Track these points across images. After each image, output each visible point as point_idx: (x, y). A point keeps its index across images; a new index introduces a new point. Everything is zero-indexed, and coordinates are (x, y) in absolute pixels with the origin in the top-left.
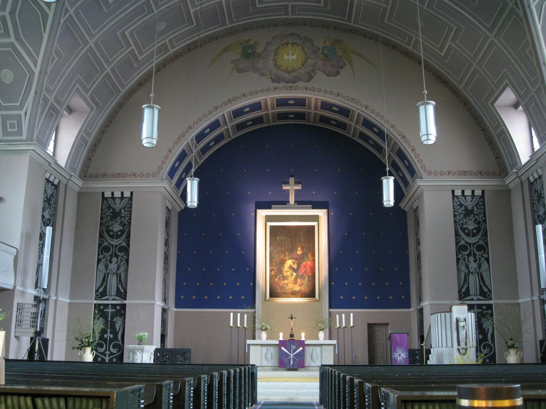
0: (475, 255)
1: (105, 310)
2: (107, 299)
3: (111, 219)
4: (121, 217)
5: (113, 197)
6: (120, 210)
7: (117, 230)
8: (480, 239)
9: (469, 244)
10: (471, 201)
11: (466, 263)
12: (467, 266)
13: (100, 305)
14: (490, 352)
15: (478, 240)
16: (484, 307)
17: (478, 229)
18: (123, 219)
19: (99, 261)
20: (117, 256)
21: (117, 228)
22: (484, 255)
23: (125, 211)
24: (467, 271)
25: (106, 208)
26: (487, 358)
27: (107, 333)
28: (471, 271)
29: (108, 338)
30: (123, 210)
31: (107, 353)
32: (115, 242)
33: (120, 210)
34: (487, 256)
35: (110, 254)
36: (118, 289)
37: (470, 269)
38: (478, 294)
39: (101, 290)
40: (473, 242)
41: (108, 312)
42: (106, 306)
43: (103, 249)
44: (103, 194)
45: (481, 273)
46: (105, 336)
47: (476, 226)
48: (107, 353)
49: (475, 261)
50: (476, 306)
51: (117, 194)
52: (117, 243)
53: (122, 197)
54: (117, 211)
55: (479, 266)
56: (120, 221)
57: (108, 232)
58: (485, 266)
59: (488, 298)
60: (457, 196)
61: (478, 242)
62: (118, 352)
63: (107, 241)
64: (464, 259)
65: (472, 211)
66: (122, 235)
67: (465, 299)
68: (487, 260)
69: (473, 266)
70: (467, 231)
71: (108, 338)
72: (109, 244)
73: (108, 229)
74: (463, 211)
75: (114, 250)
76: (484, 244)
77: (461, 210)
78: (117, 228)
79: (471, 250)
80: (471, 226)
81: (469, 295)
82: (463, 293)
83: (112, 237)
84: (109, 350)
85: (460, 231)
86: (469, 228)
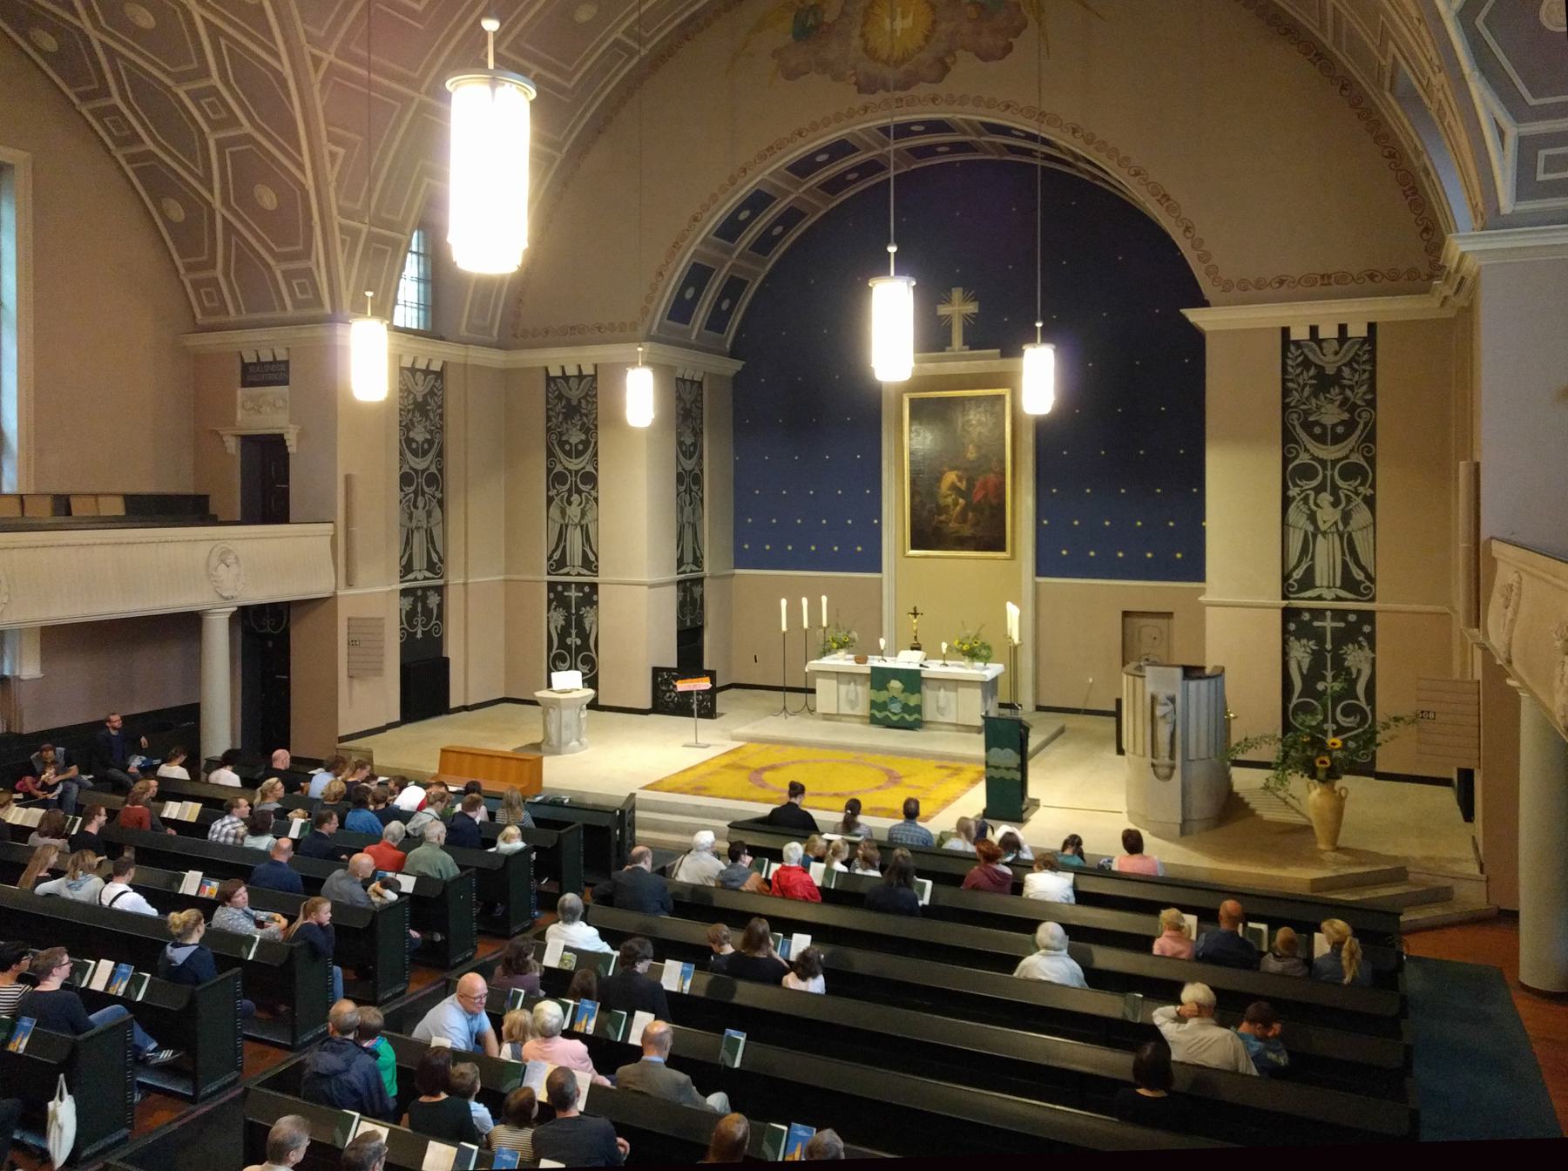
0: (1335, 490)
1: (1316, 624)
2: (568, 574)
4: (1343, 387)
5: (565, 378)
8: (1352, 451)
9: (1323, 462)
12: (1312, 518)
17: (1350, 426)
18: (1348, 392)
19: (550, 500)
20: (579, 492)
21: (575, 437)
22: (1361, 489)
23: (1354, 370)
27: (1324, 678)
28: (1323, 527)
30: (1346, 372)
32: (1329, 453)
33: (1339, 370)
36: (584, 552)
37: (1320, 523)
38: (1338, 583)
39: (556, 556)
42: (567, 585)
44: (1285, 332)
45: (1350, 535)
46: (1320, 686)
49: (1335, 504)
50: (1328, 614)
51: (1328, 332)
53: (581, 377)
54: (1330, 370)
55: (1346, 517)
57: (1308, 426)
58: (1361, 516)
59: (1363, 595)
60: (1297, 343)
64: (1306, 500)
65: (1337, 378)
68: (1370, 502)
69: (1328, 515)
72: (1314, 458)
78: (575, 437)
79: (1325, 476)
80: (1331, 415)
81: (1312, 586)
83: (1321, 439)
84: (1335, 721)
85: (1299, 429)
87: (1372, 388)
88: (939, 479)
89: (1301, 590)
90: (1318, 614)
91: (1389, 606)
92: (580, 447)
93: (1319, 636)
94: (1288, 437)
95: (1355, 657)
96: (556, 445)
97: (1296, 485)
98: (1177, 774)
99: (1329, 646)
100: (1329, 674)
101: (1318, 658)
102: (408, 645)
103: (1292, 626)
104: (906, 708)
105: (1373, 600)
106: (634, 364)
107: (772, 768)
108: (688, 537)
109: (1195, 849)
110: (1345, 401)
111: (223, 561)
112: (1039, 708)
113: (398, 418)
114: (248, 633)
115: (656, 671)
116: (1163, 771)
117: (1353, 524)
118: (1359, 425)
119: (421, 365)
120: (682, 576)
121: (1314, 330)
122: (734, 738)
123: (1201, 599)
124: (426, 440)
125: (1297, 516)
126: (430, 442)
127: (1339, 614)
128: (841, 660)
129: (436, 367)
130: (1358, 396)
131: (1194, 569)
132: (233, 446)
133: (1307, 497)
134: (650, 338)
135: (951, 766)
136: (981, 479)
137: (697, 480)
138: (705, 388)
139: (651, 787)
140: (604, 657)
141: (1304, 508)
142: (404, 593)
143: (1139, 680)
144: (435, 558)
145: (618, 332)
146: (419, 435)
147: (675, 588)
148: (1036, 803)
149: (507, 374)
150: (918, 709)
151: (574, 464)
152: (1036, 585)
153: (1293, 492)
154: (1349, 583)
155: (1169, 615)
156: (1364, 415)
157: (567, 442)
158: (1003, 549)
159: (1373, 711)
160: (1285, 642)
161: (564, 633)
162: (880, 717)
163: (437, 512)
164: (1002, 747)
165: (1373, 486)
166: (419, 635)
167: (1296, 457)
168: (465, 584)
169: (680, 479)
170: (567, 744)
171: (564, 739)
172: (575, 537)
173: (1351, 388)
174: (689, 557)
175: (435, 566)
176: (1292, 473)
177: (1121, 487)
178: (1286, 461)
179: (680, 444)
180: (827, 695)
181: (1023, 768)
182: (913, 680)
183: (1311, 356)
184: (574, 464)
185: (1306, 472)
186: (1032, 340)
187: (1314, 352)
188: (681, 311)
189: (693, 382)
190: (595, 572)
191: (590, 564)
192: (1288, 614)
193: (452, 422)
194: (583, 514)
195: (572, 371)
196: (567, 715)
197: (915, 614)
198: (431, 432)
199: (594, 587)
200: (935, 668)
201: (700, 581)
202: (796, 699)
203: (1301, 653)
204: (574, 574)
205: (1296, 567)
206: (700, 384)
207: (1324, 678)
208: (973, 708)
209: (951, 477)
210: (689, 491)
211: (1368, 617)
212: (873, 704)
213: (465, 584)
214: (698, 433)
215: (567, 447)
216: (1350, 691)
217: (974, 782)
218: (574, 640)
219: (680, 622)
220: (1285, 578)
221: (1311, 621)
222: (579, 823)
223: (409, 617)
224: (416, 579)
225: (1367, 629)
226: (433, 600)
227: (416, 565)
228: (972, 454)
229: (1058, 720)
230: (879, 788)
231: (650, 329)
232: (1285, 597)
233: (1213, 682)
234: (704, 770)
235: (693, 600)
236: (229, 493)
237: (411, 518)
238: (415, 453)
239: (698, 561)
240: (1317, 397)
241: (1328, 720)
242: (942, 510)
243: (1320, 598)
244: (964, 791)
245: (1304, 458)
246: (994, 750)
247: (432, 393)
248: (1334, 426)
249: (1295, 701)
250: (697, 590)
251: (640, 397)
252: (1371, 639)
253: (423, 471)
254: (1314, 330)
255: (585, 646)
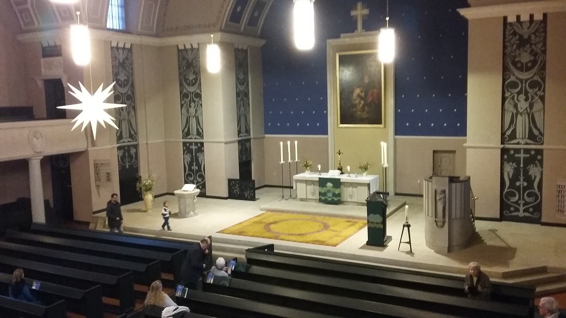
0: (526, 93)
1: (516, 155)
2: (191, 138)
3: (187, 69)
4: (531, 45)
6: (530, 36)
7: (527, 60)
8: (535, 75)
9: (521, 81)
10: (529, 28)
11: (514, 102)
12: (516, 106)
13: (187, 143)
14: (535, 201)
15: (532, 75)
16: (533, 152)
17: (534, 63)
18: (533, 46)
19: (182, 106)
20: (194, 102)
21: (191, 77)
22: (538, 93)
23: (536, 36)
24: (515, 111)
25: (511, 35)
26: (531, 207)
27: (520, 180)
28: (521, 111)
29: (522, 187)
31: (522, 202)
32: (524, 76)
33: (530, 36)
34: (542, 93)
35: (189, 99)
36: (197, 129)
37: (519, 109)
38: (527, 136)
39: (186, 130)
40: (525, 77)
41: (520, 158)
42: (191, 144)
43: (184, 96)
44: (505, 18)
45: (533, 114)
46: (518, 184)
47: (532, 58)
48: (522, 202)
49: (526, 100)
50: (522, 151)
51: (525, 18)
52: (193, 91)
54: (526, 37)
55: (531, 106)
56: (530, 49)
57: (515, 64)
58: (538, 105)
59: (537, 142)
60: (511, 24)
61: (127, 92)
62: (202, 180)
63: (514, 75)
64: (513, 98)
65: (529, 40)
66: (532, 67)
67: (510, 142)
68: (542, 98)
69: (523, 105)
70: (519, 65)
71: (522, 187)
72: (517, 78)
73: (514, 60)
74: (517, 40)
75: (524, 85)
76: (540, 80)
77: (515, 39)
78: (191, 77)
79: (522, 87)
80: (525, 58)
81: (515, 138)
82: (508, 136)
83: (521, 69)
84: (524, 199)
85: (511, 65)
86: (522, 61)
87: (545, 45)
88: (352, 92)
89: (509, 140)
90: (517, 151)
91: (551, 147)
92: (125, 82)
93: (517, 161)
94: (505, 69)
95: (534, 171)
96: (183, 81)
97: (508, 91)
98: (446, 225)
99: (522, 166)
100: (522, 178)
101: (517, 171)
102: (122, 171)
103: (506, 157)
104: (334, 195)
105: (542, 144)
106: (210, 43)
107: (275, 223)
108: (243, 119)
109: (453, 258)
110: (532, 51)
111: (35, 136)
112: (396, 194)
113: (111, 70)
114: (53, 168)
115: (230, 181)
116: (440, 224)
117: (535, 108)
118: (538, 63)
119: (121, 45)
120: (240, 138)
121: (518, 17)
122: (261, 210)
123: (464, 145)
124: (125, 80)
125: (509, 106)
126: (127, 81)
127: (527, 151)
128: (307, 175)
129: (128, 46)
130: (538, 48)
131: (462, 131)
132: (41, 84)
133: (514, 97)
134: (221, 30)
135: (351, 220)
136: (371, 92)
137: (247, 95)
138: (249, 52)
139: (222, 232)
140: (208, 175)
141: (512, 102)
142: (119, 148)
143: (430, 183)
144: (132, 132)
145: (206, 29)
146: (122, 77)
147: (237, 144)
148: (390, 238)
149: (160, 49)
150: (339, 195)
151: (192, 89)
152: (395, 140)
153: (507, 94)
154: (531, 136)
155: (454, 152)
156: (540, 57)
157: (188, 79)
158: (381, 123)
159: (541, 194)
160: (502, 164)
161: (191, 164)
162: (324, 200)
163: (132, 112)
164: (375, 214)
165: (544, 91)
166: (127, 167)
167: (510, 77)
168: (147, 144)
169: (238, 95)
170: (189, 213)
171: (187, 211)
172: (193, 122)
173: (535, 45)
174: (243, 129)
175: (133, 136)
176: (506, 86)
177: (430, 96)
178: (504, 80)
179: (237, 79)
180: (301, 190)
181: (384, 223)
182: (337, 183)
183: (517, 30)
184: (192, 89)
185: (514, 85)
186: (384, 26)
187: (518, 27)
188: (235, 17)
189: (243, 50)
190: (202, 137)
191: (200, 134)
192: (504, 151)
193: (136, 72)
194: (196, 111)
195: (188, 47)
196: (188, 201)
197: (340, 154)
198: (127, 76)
199: (202, 144)
200: (344, 178)
201: (249, 140)
202: (287, 191)
203: (509, 169)
204: (194, 139)
205: (508, 129)
206: (246, 51)
207: (520, 180)
208: (363, 195)
209: (358, 91)
210: (242, 100)
211: (540, 152)
212: (320, 194)
213: (147, 144)
214: (246, 74)
215: (188, 81)
216: (531, 185)
217: (361, 228)
218: (195, 168)
219: (240, 158)
220: (503, 134)
221: (514, 154)
222: (182, 250)
223: (122, 159)
224: (124, 142)
225: (539, 157)
226: (133, 151)
227: (124, 136)
228: (366, 80)
229: (402, 199)
230: (318, 231)
231: (221, 26)
232: (502, 143)
233: (463, 184)
234: (247, 223)
235: (246, 149)
236: (41, 107)
237: (120, 115)
238: (120, 86)
239: (248, 131)
240: (519, 49)
241: (521, 198)
242: (355, 106)
243: (518, 143)
244: (355, 232)
245: (513, 78)
246: (371, 215)
247: (127, 58)
248: (527, 63)
249: (506, 190)
250: (247, 144)
251: (214, 59)
252: (541, 162)
253: (125, 94)
254: (518, 17)
255: (199, 170)
